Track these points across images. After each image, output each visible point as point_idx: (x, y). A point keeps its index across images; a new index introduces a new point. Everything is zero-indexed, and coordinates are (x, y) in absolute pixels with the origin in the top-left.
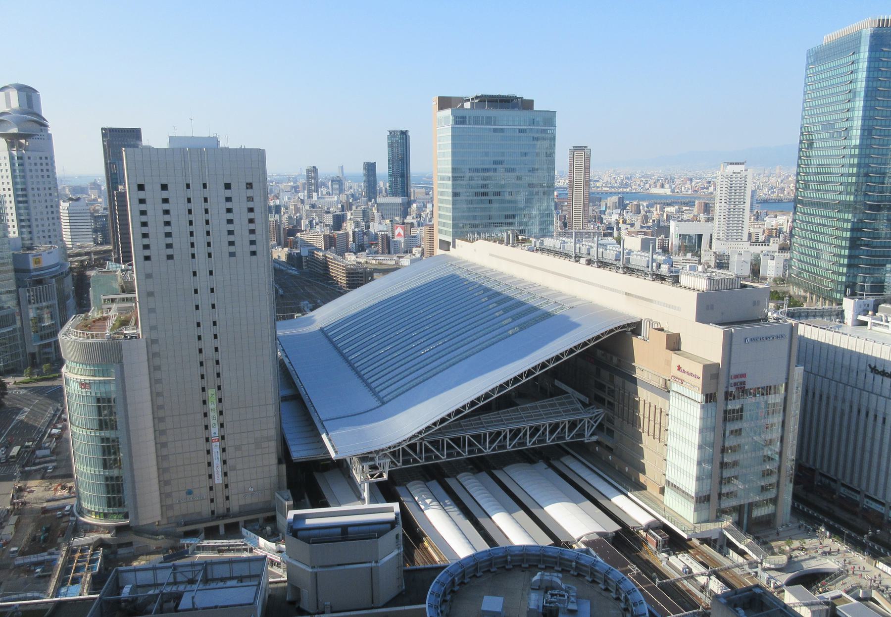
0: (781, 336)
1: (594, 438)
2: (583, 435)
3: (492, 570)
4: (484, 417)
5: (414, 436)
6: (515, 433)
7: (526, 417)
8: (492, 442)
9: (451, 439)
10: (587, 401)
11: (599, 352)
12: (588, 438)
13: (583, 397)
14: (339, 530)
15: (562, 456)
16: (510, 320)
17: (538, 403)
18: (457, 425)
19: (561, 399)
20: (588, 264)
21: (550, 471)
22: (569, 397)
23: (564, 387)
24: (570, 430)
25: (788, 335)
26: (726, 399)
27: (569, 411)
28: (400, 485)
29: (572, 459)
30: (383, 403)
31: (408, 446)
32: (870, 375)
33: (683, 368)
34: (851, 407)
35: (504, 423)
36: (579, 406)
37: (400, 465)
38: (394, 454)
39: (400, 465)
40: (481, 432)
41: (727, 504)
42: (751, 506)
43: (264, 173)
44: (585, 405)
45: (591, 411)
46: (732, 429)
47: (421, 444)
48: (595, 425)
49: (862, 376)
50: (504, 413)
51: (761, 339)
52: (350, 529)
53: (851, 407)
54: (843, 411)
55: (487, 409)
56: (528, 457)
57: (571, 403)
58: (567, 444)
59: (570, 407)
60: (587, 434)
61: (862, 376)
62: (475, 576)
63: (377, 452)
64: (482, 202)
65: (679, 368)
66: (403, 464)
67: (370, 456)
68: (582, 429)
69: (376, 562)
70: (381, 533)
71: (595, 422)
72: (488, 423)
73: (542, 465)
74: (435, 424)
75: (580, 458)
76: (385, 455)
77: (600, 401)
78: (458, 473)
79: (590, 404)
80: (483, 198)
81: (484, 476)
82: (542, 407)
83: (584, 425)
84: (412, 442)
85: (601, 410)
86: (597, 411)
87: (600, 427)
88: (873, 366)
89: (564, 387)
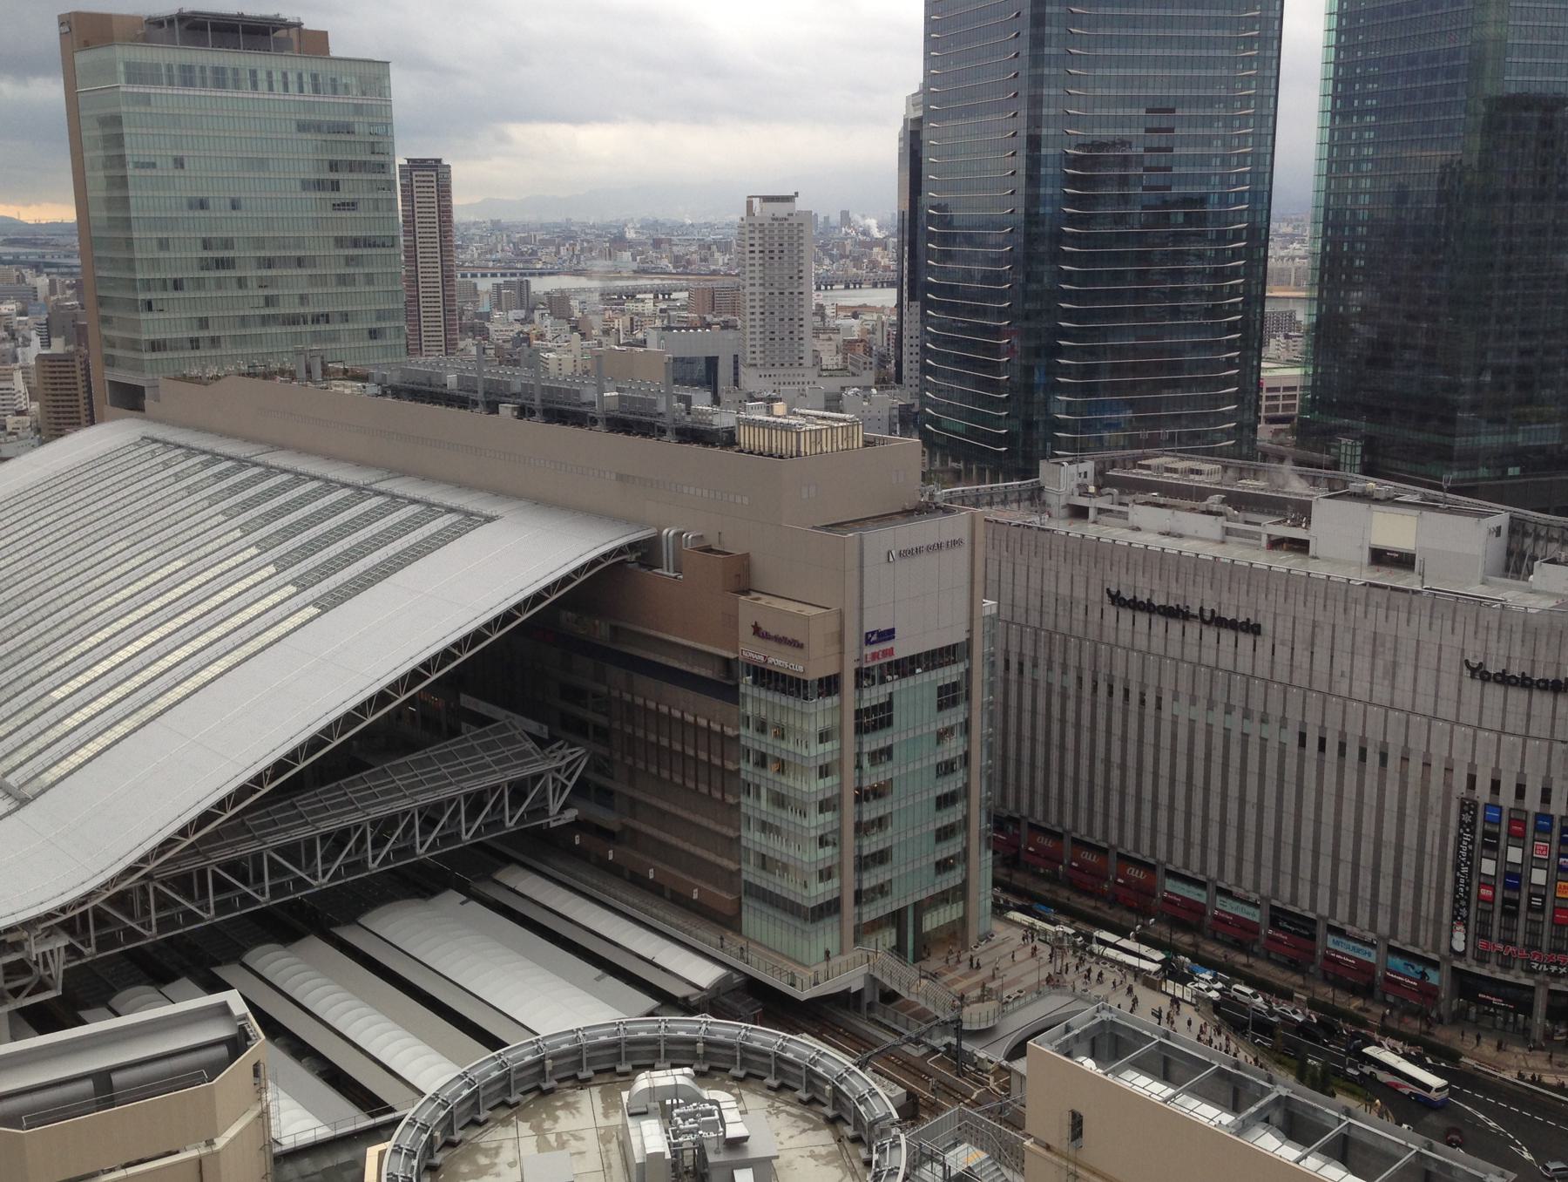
0: (954, 543)
1: (571, 815)
2: (544, 812)
3: (512, 1100)
4: (303, 801)
5: (131, 870)
6: (476, 802)
7: (408, 787)
8: (328, 858)
9: (277, 850)
10: (544, 732)
11: (567, 616)
12: (559, 814)
13: (533, 726)
14: (88, 1085)
15: (498, 868)
16: (272, 569)
17: (430, 752)
18: (237, 828)
19: (486, 734)
20: (520, 417)
21: (474, 905)
22: (504, 728)
23: (484, 708)
24: (471, 817)
25: (966, 540)
26: (858, 685)
27: (507, 759)
28: (228, 961)
29: (522, 872)
30: (24, 802)
31: (110, 901)
32: (1111, 611)
33: (765, 627)
34: (1080, 679)
35: (357, 807)
36: (529, 745)
37: (90, 952)
38: (68, 927)
39: (90, 952)
40: (301, 834)
41: (871, 912)
42: (920, 908)
43: (445, 212)
44: (541, 743)
45: (560, 754)
46: (874, 747)
47: (144, 889)
48: (570, 785)
49: (1095, 615)
50: (352, 784)
51: (919, 550)
52: (117, 1078)
53: (1080, 679)
54: (1064, 689)
55: (297, 785)
56: (417, 883)
57: (510, 741)
58: (509, 839)
59: (507, 751)
60: (554, 808)
61: (1095, 615)
62: (504, 1104)
63: (28, 925)
64: (220, 284)
65: (757, 630)
66: (99, 949)
67: (10, 938)
68: (542, 797)
69: (210, 1143)
70: (215, 1069)
71: (569, 778)
72: (315, 812)
73: (452, 898)
74: (183, 832)
75: (546, 869)
76: (50, 933)
77: (575, 729)
78: (245, 950)
79: (554, 739)
80: (222, 273)
81: (315, 946)
82: (443, 758)
83: (544, 789)
84: (122, 886)
85: (580, 751)
86: (571, 753)
87: (581, 789)
88: (1114, 590)
89: (484, 708)
